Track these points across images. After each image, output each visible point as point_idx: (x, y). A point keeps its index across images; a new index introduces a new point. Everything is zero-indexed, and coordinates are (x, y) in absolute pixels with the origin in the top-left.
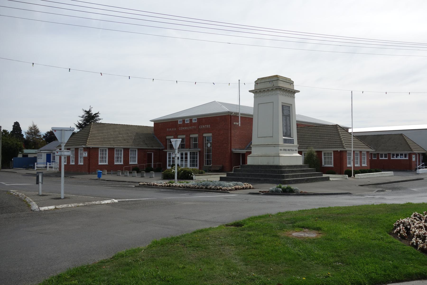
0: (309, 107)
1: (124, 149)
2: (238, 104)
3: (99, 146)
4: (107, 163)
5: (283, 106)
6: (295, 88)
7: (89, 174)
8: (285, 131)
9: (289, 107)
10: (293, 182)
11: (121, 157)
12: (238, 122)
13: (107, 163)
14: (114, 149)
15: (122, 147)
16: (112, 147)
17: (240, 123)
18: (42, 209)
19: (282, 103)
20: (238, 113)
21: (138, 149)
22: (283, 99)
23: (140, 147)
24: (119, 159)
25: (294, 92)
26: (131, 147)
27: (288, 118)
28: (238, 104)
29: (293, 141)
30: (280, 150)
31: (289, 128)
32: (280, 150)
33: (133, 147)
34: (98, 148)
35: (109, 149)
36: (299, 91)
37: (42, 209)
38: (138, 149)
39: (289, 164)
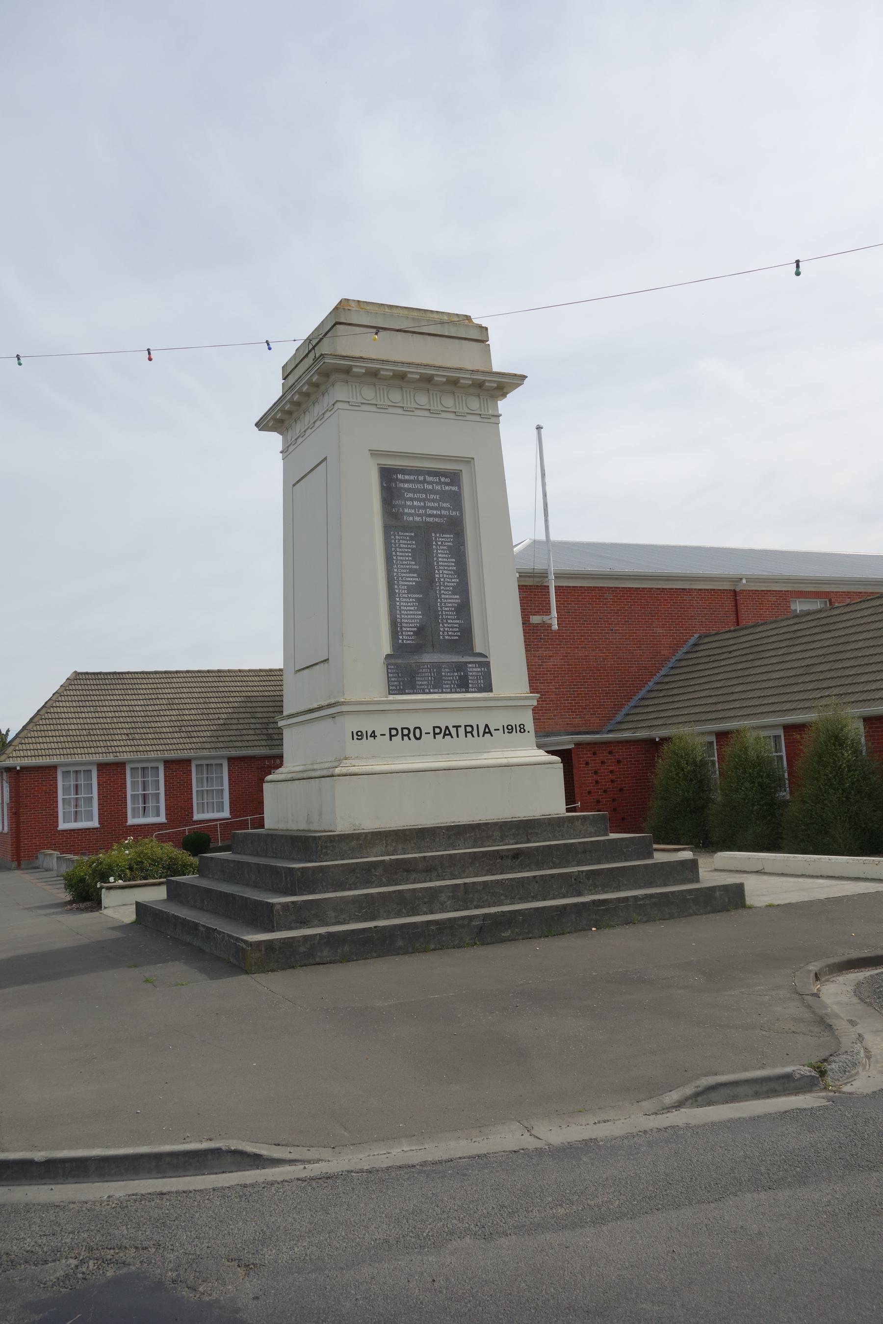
0: (604, 476)
1: (168, 763)
2: (544, 538)
3: (192, 754)
4: (95, 823)
5: (388, 475)
6: (501, 360)
7: (19, 867)
8: (412, 616)
9: (454, 478)
10: (326, 953)
11: (157, 795)
12: (548, 611)
13: (95, 823)
14: (121, 765)
15: (152, 755)
16: (111, 758)
17: (554, 613)
18: (687, 855)
19: (374, 453)
20: (544, 575)
21: (231, 760)
22: (424, 434)
23: (234, 753)
24: (151, 804)
25: (505, 384)
26: (62, 759)
27: (442, 543)
28: (542, 537)
29: (487, 676)
30: (359, 735)
31: (448, 600)
32: (359, 735)
33: (206, 753)
34: (53, 768)
35: (103, 767)
36: (520, 379)
37: (687, 855)
38: (231, 760)
39: (464, 818)
